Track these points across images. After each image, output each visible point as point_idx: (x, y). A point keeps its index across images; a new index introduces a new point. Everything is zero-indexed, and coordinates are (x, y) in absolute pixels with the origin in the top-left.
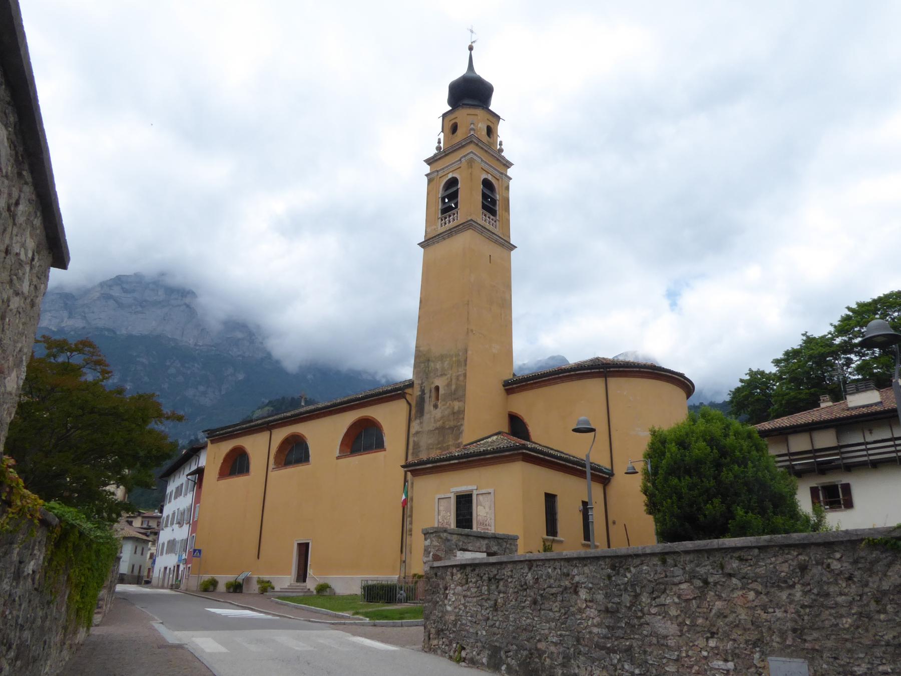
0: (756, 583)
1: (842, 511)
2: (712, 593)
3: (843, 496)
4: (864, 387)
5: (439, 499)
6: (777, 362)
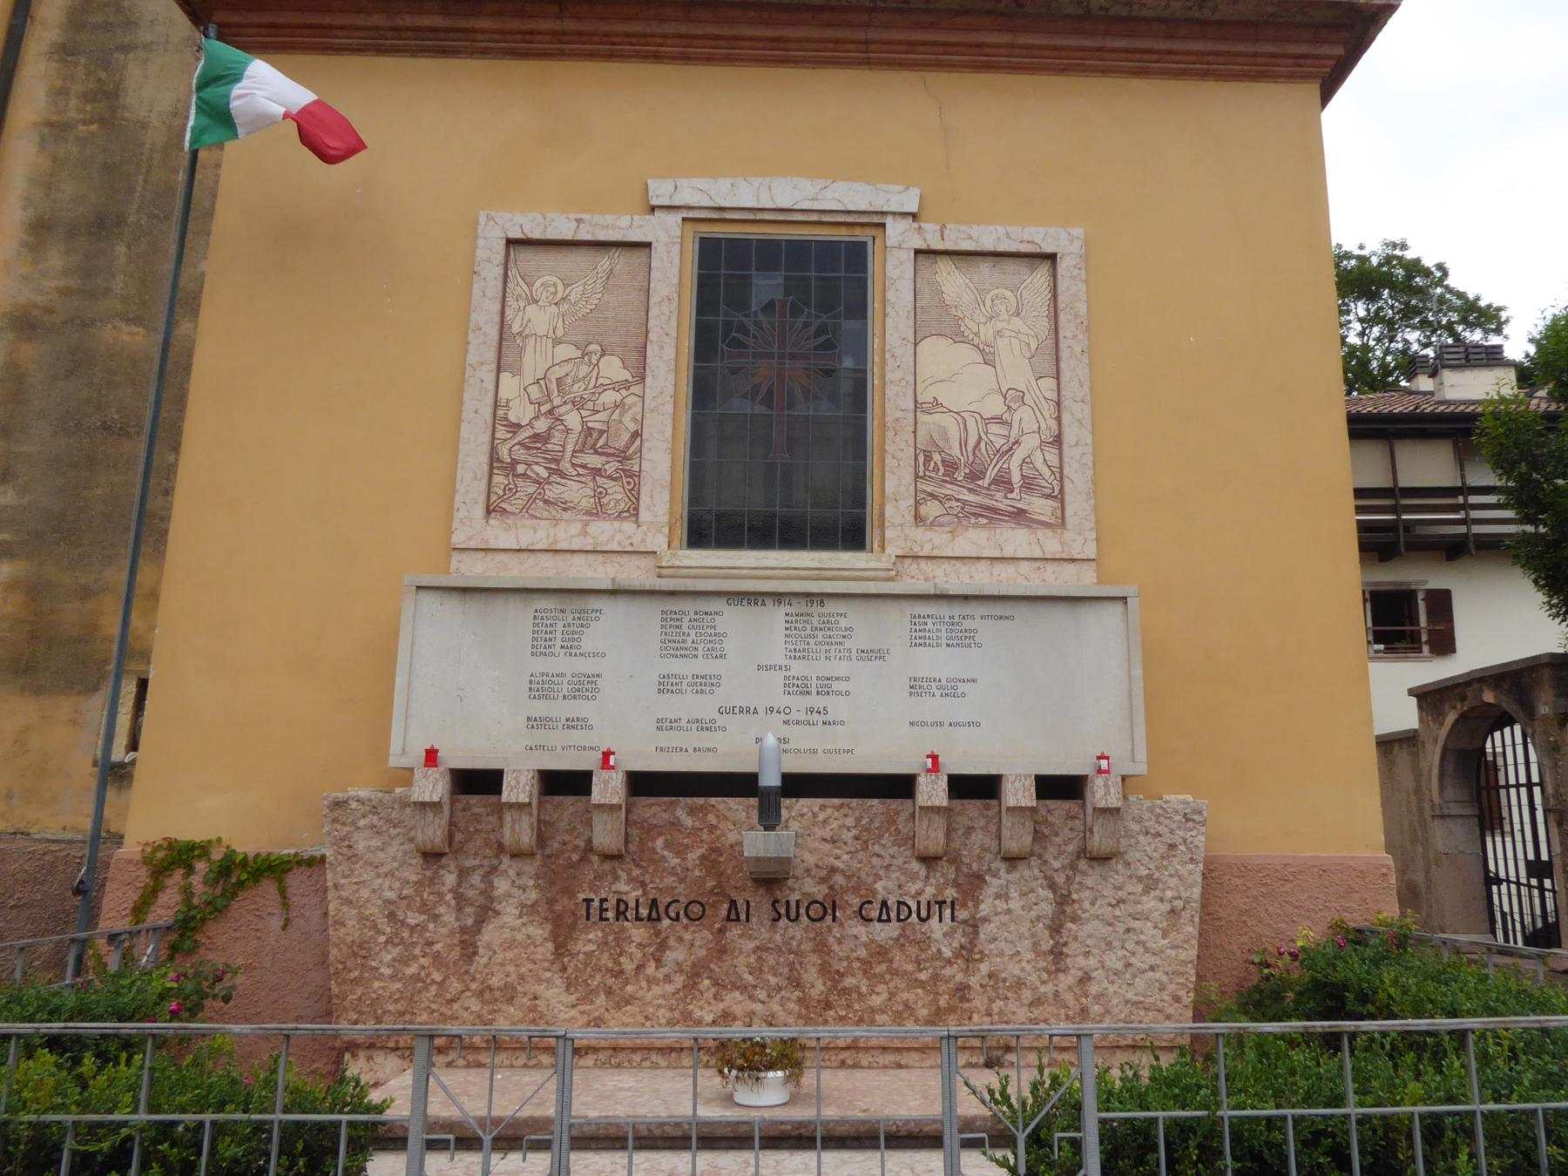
0: (529, 903)
1: (1425, 659)
2: (600, 934)
3: (1430, 620)
4: (1483, 356)
5: (511, 243)
6: (1339, 246)
